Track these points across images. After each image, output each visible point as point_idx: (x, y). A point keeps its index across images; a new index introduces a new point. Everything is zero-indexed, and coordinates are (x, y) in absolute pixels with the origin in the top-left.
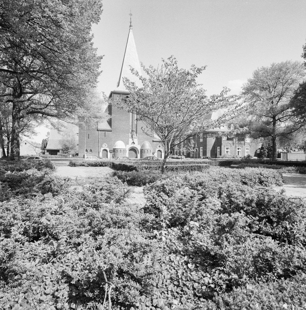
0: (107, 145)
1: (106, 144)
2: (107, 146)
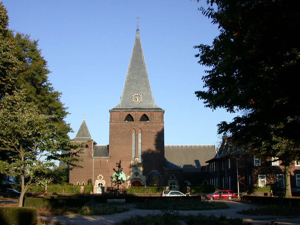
0: (102, 177)
1: (101, 175)
2: (102, 178)
